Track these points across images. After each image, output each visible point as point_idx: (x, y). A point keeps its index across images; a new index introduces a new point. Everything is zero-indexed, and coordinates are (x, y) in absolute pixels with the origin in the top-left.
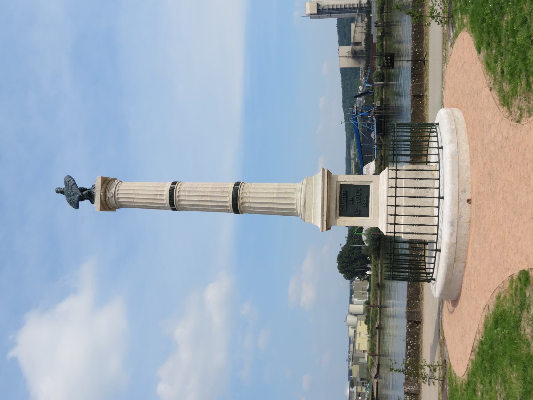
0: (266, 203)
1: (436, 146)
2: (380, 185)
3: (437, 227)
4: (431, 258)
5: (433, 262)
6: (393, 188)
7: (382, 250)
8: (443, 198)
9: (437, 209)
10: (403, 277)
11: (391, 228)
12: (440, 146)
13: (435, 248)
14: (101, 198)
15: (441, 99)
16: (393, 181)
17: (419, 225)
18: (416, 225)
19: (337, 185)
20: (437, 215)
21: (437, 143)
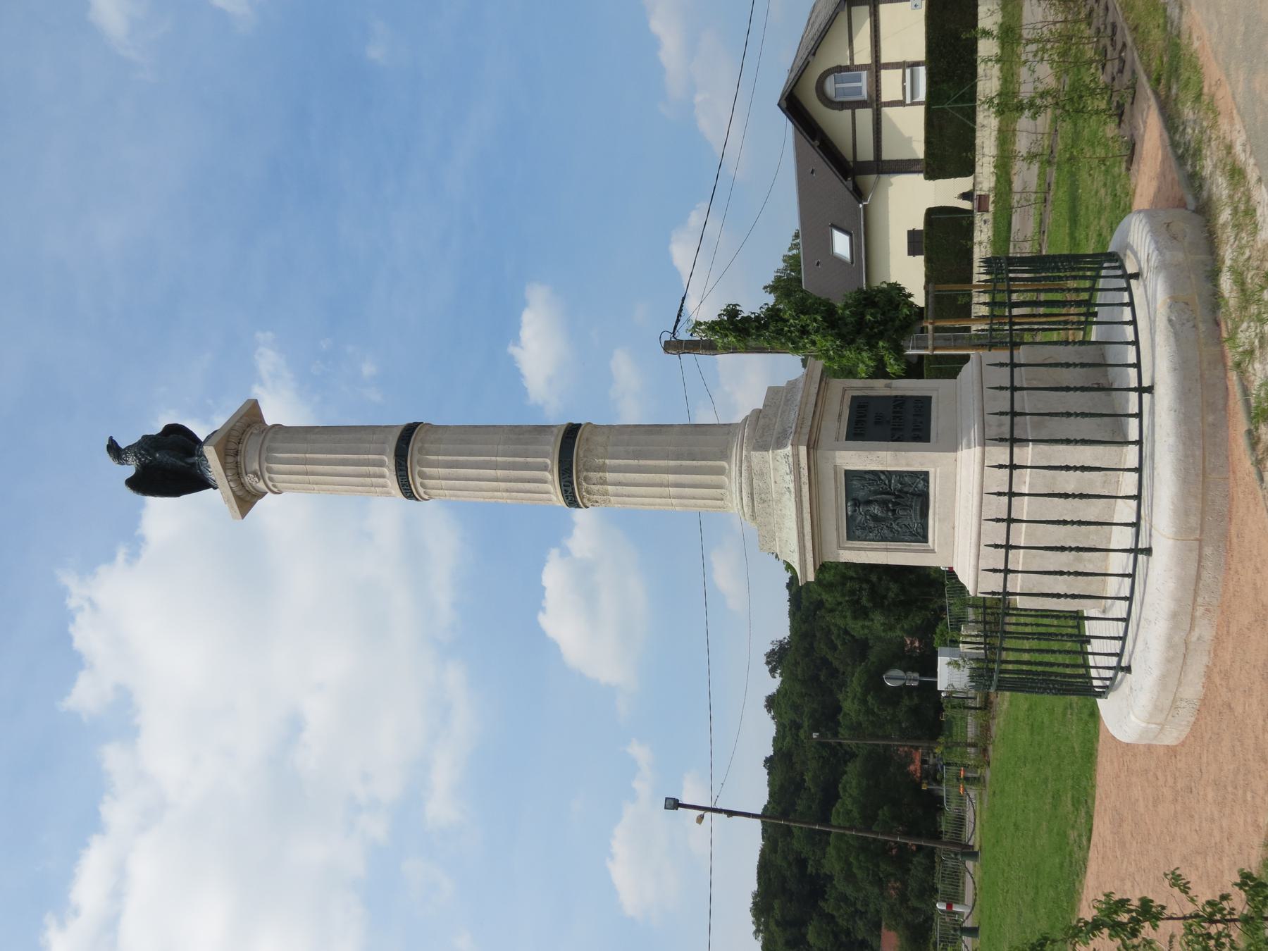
0: (661, 485)
1: (1129, 544)
2: (958, 489)
3: (1128, 602)
4: (1124, 368)
5: (1131, 338)
6: (1002, 498)
7: (1065, 21)
8: (1150, 390)
9: (1135, 476)
10: (1073, 274)
11: (993, 583)
12: (1146, 383)
13: (1134, 384)
14: (234, 492)
15: (1149, 336)
16: (1004, 460)
17: (1078, 549)
18: (1071, 549)
19: (836, 473)
20: (1136, 410)
21: (1124, 624)
